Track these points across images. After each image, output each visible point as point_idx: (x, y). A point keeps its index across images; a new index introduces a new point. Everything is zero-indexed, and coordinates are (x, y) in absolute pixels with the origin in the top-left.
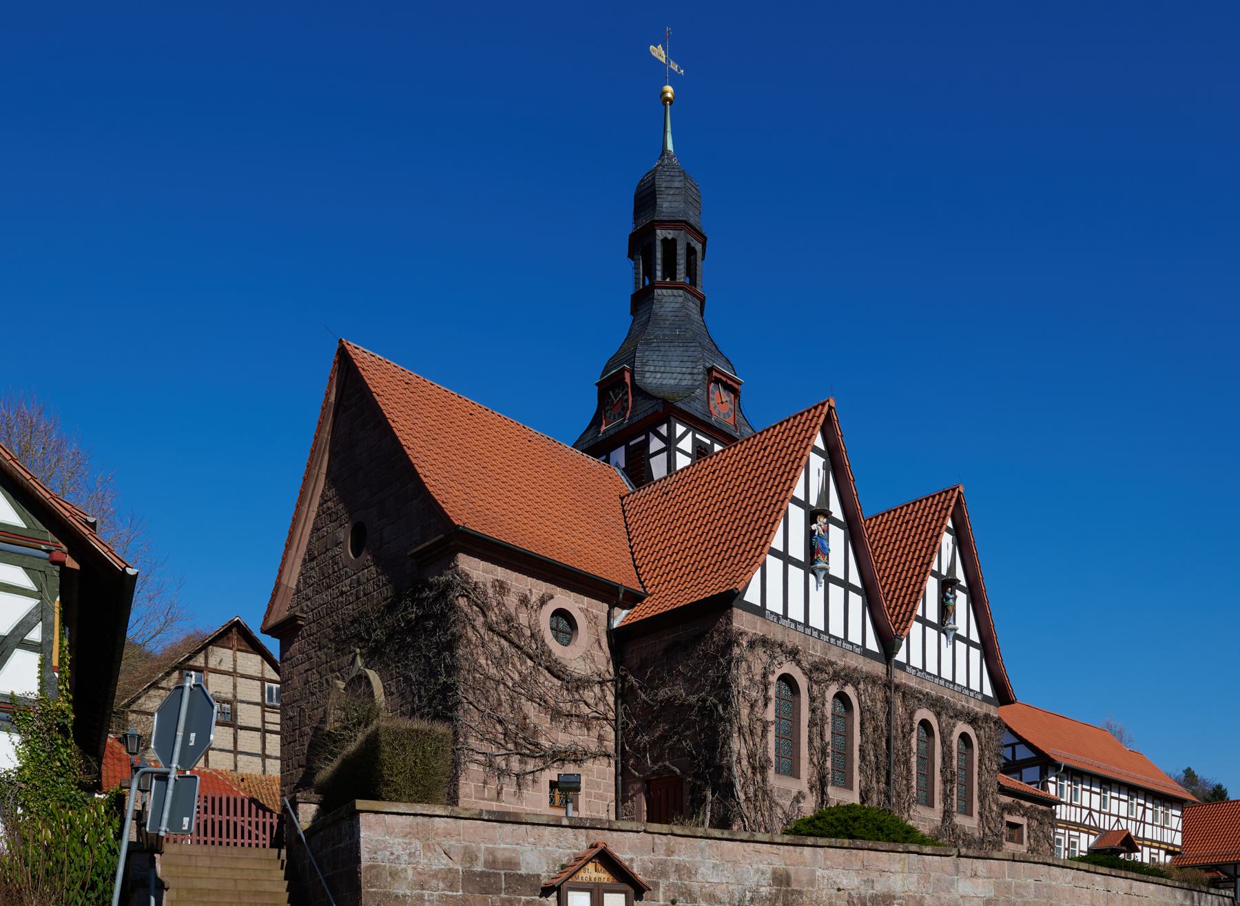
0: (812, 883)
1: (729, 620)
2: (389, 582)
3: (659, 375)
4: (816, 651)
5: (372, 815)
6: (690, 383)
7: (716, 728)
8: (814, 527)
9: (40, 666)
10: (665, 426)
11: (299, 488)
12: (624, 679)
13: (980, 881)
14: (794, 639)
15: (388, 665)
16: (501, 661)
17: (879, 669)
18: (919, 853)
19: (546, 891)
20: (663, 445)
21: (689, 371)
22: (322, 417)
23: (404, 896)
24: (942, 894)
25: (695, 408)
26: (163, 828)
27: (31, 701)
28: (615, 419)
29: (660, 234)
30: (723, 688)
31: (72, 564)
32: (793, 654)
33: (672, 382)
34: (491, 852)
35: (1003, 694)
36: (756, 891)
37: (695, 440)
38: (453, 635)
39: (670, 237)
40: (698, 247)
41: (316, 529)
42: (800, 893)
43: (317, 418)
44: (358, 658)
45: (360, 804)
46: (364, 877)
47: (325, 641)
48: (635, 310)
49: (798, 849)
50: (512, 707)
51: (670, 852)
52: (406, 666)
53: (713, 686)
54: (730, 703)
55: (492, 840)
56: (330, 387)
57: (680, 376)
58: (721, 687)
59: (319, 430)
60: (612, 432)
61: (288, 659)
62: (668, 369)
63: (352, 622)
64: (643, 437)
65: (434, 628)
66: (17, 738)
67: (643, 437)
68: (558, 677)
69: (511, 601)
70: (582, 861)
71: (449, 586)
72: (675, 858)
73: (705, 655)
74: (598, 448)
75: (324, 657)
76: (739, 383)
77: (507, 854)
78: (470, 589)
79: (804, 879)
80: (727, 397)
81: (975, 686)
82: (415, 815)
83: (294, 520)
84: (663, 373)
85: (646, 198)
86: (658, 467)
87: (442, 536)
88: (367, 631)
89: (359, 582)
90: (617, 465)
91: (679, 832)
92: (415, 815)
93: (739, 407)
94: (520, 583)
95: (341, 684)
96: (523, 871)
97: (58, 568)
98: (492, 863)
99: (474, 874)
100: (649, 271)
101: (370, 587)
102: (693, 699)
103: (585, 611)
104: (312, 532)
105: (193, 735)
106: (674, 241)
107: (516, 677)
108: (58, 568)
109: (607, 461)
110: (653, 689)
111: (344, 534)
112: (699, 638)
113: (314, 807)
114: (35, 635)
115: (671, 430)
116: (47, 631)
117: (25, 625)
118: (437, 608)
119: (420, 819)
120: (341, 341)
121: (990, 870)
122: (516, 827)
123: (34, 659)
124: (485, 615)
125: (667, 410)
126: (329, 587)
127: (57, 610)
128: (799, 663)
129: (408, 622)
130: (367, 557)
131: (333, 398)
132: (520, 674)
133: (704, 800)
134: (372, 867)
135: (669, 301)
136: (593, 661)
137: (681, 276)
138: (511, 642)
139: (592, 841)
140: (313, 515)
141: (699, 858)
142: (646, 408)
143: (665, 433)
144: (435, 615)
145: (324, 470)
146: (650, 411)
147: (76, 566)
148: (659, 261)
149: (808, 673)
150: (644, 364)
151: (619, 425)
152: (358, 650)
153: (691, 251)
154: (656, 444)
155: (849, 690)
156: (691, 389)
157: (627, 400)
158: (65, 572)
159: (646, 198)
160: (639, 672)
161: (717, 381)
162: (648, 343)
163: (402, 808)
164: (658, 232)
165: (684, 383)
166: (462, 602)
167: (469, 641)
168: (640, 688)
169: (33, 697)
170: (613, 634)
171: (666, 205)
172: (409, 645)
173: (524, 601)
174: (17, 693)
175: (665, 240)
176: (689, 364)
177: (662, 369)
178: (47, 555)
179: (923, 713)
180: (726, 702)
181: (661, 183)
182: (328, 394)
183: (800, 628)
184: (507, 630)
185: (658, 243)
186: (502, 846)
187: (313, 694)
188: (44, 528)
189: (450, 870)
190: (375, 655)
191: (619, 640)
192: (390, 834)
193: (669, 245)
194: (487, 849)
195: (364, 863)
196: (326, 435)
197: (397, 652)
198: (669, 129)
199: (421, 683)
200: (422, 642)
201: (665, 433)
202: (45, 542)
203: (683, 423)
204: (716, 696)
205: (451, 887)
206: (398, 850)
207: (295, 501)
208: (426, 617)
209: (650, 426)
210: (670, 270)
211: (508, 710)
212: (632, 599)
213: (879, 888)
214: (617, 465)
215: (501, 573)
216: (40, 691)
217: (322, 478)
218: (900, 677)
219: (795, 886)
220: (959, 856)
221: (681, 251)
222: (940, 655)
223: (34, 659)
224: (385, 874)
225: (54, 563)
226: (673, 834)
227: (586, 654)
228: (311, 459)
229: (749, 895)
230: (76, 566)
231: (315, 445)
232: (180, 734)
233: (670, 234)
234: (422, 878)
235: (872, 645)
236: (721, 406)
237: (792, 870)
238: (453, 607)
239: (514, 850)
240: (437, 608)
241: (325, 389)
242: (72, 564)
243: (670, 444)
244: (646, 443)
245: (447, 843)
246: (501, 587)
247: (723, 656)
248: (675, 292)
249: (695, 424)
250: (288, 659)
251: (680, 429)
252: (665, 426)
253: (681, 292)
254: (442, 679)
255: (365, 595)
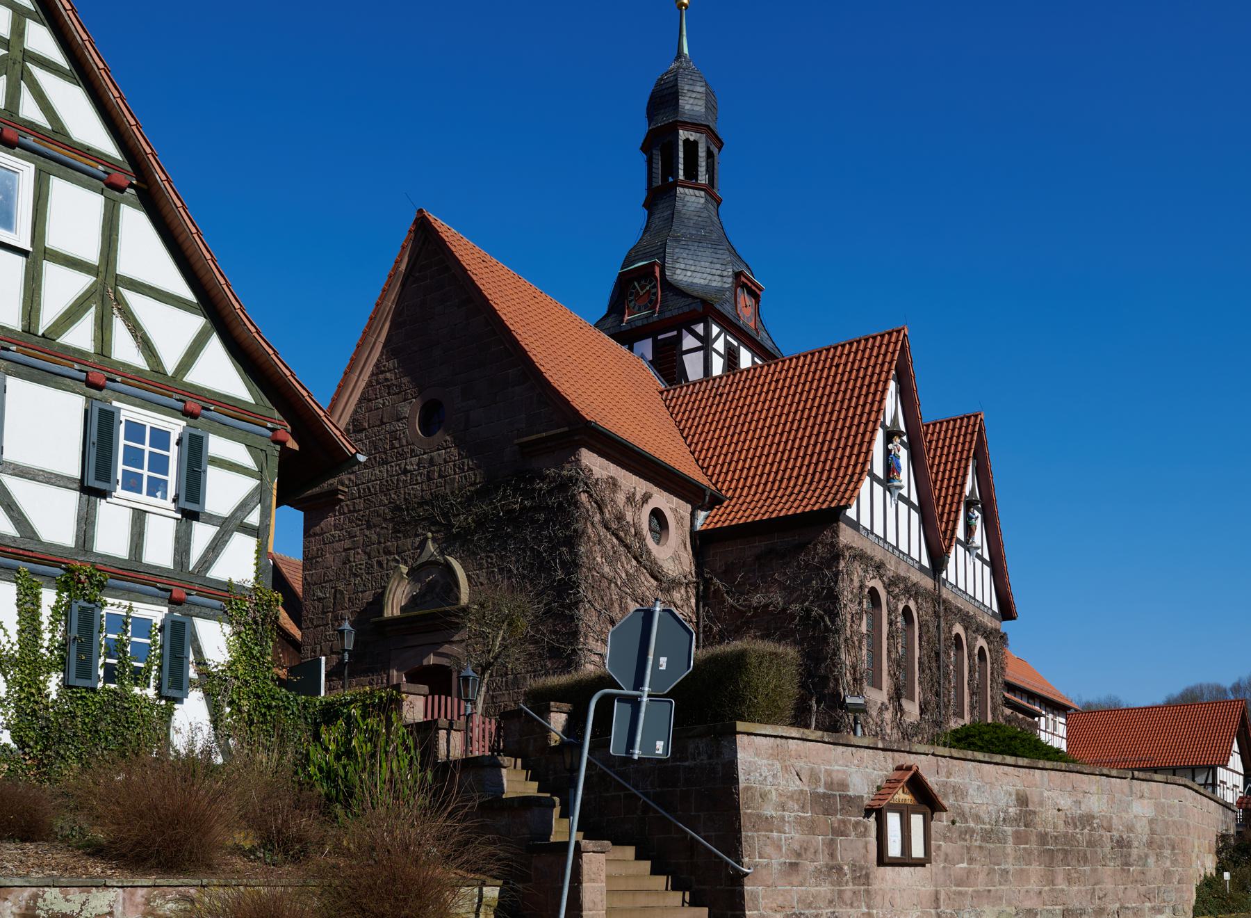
0: (1041, 804)
1: (836, 533)
2: (479, 467)
3: (689, 274)
4: (892, 568)
5: (746, 737)
6: (719, 284)
7: (826, 638)
8: (890, 446)
9: (257, 551)
10: (702, 325)
11: (350, 353)
12: (707, 582)
13: (1146, 801)
14: (878, 554)
15: (475, 554)
16: (612, 560)
17: (927, 583)
18: (1108, 776)
19: (868, 813)
20: (699, 344)
21: (719, 272)
22: (389, 284)
23: (772, 817)
24: (1124, 814)
25: (727, 310)
26: (637, 751)
27: (247, 589)
28: (639, 311)
29: (683, 134)
30: (831, 598)
31: (292, 444)
32: (879, 567)
33: (702, 282)
34: (828, 773)
35: (1006, 611)
36: (1006, 812)
37: (726, 342)
38: (576, 531)
39: (692, 139)
40: (715, 151)
41: (364, 398)
42: (1035, 813)
43: (382, 284)
44: (430, 543)
45: (740, 726)
46: (743, 798)
47: (376, 520)
48: (650, 204)
49: (1032, 771)
50: (620, 605)
51: (949, 774)
52: (502, 558)
53: (817, 593)
54: (837, 615)
55: (829, 763)
56: (401, 256)
57: (710, 277)
58: (826, 598)
59: (383, 297)
60: (639, 323)
61: (315, 535)
62: (698, 269)
63: (420, 505)
64: (675, 333)
65: (547, 521)
66: (228, 629)
67: (675, 333)
68: (656, 578)
69: (621, 498)
70: (892, 783)
71: (573, 481)
72: (952, 779)
73: (807, 565)
74: (627, 338)
75: (375, 538)
76: (761, 289)
77: (840, 776)
78: (590, 485)
79: (1036, 800)
80: (750, 301)
81: (987, 603)
82: (776, 737)
83: (339, 386)
84: (695, 271)
85: (664, 98)
86: (693, 366)
87: (566, 429)
88: (445, 515)
89: (432, 462)
90: (642, 357)
91: (955, 755)
92: (776, 737)
93: (757, 312)
94: (630, 482)
95: (404, 569)
96: (851, 793)
97: (278, 447)
98: (830, 785)
99: (818, 795)
100: (670, 168)
101: (449, 469)
102: (795, 608)
103: (674, 511)
104: (360, 401)
105: (663, 660)
106: (695, 143)
107: (624, 575)
108: (278, 447)
109: (631, 349)
110: (742, 594)
111: (411, 409)
112: (801, 547)
113: (564, 716)
114: (254, 518)
115: (708, 330)
116: (265, 515)
117: (244, 507)
118: (552, 501)
119: (778, 741)
120: (420, 211)
121: (1152, 792)
122: (844, 749)
123: (251, 543)
124: (602, 513)
125: (703, 310)
126: (385, 462)
127: (275, 492)
128: (881, 577)
129: (509, 512)
130: (442, 437)
131: (403, 267)
132: (627, 572)
133: (810, 709)
134: (747, 789)
135: (691, 199)
136: (680, 563)
137: (703, 178)
138: (618, 537)
139: (897, 764)
140: (362, 385)
141: (967, 780)
142: (677, 307)
143: (701, 333)
144: (547, 508)
145: (383, 338)
146: (686, 309)
147: (296, 447)
148: (681, 161)
149: (886, 587)
150: (675, 261)
151: (647, 317)
152: (430, 535)
153: (710, 154)
154: (689, 342)
155: (912, 604)
156: (721, 291)
157: (655, 294)
158: (285, 452)
159: (664, 98)
160: (727, 573)
161: (744, 286)
162: (677, 240)
163: (768, 729)
164: (681, 132)
165: (714, 284)
166: (584, 497)
167: (589, 537)
168: (727, 593)
169: (249, 585)
170: (694, 535)
171: (687, 107)
172: (509, 536)
173: (630, 499)
174: (235, 580)
175: (687, 141)
176: (718, 266)
177: (693, 268)
178: (270, 434)
179: (958, 629)
180: (834, 615)
181: (684, 86)
182: (398, 263)
183: (881, 543)
184: (618, 528)
185: (681, 143)
186: (837, 768)
187: (356, 575)
188: (270, 405)
189: (802, 791)
190: (453, 540)
191: (702, 543)
192: (757, 755)
193: (691, 147)
194: (826, 770)
195: (742, 785)
196: (390, 303)
197: (488, 542)
198: (684, 33)
199: (524, 577)
200: (528, 533)
201: (701, 333)
202: (271, 420)
203: (718, 325)
204: (819, 606)
205: (803, 808)
206: (765, 772)
207: (344, 367)
208: (535, 509)
209: (686, 323)
210: (691, 172)
211: (618, 610)
212: (715, 501)
213: (1084, 809)
214: (642, 357)
215: (613, 470)
216: (257, 578)
217: (379, 347)
218: (946, 593)
219: (1031, 808)
220: (1133, 778)
221: (702, 153)
222: (968, 575)
223: (251, 543)
224: (757, 795)
225: (276, 442)
226: (951, 757)
227: (673, 555)
228: (369, 326)
229: (1002, 815)
230: (296, 447)
231: (376, 312)
232: (651, 657)
233: (693, 136)
234: (783, 799)
235: (925, 562)
236: (745, 310)
237: (1028, 790)
238: (576, 504)
239: (844, 772)
240: (552, 501)
241: (396, 256)
242: (292, 444)
243: (706, 344)
244: (679, 340)
245: (800, 764)
246: (613, 484)
247: (829, 568)
248: (697, 192)
249: (730, 326)
250: (315, 535)
251: (715, 330)
252: (702, 325)
253: (702, 193)
254: (560, 574)
255: (440, 476)
